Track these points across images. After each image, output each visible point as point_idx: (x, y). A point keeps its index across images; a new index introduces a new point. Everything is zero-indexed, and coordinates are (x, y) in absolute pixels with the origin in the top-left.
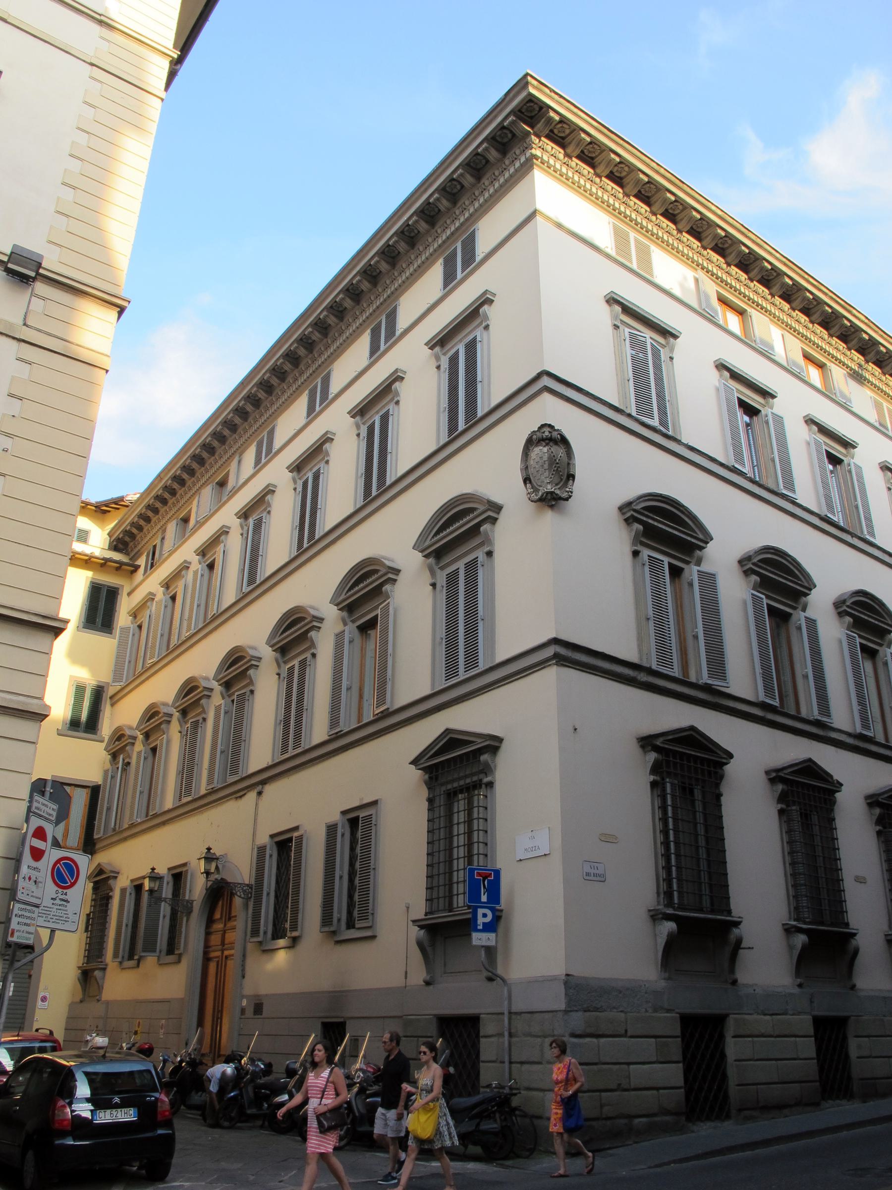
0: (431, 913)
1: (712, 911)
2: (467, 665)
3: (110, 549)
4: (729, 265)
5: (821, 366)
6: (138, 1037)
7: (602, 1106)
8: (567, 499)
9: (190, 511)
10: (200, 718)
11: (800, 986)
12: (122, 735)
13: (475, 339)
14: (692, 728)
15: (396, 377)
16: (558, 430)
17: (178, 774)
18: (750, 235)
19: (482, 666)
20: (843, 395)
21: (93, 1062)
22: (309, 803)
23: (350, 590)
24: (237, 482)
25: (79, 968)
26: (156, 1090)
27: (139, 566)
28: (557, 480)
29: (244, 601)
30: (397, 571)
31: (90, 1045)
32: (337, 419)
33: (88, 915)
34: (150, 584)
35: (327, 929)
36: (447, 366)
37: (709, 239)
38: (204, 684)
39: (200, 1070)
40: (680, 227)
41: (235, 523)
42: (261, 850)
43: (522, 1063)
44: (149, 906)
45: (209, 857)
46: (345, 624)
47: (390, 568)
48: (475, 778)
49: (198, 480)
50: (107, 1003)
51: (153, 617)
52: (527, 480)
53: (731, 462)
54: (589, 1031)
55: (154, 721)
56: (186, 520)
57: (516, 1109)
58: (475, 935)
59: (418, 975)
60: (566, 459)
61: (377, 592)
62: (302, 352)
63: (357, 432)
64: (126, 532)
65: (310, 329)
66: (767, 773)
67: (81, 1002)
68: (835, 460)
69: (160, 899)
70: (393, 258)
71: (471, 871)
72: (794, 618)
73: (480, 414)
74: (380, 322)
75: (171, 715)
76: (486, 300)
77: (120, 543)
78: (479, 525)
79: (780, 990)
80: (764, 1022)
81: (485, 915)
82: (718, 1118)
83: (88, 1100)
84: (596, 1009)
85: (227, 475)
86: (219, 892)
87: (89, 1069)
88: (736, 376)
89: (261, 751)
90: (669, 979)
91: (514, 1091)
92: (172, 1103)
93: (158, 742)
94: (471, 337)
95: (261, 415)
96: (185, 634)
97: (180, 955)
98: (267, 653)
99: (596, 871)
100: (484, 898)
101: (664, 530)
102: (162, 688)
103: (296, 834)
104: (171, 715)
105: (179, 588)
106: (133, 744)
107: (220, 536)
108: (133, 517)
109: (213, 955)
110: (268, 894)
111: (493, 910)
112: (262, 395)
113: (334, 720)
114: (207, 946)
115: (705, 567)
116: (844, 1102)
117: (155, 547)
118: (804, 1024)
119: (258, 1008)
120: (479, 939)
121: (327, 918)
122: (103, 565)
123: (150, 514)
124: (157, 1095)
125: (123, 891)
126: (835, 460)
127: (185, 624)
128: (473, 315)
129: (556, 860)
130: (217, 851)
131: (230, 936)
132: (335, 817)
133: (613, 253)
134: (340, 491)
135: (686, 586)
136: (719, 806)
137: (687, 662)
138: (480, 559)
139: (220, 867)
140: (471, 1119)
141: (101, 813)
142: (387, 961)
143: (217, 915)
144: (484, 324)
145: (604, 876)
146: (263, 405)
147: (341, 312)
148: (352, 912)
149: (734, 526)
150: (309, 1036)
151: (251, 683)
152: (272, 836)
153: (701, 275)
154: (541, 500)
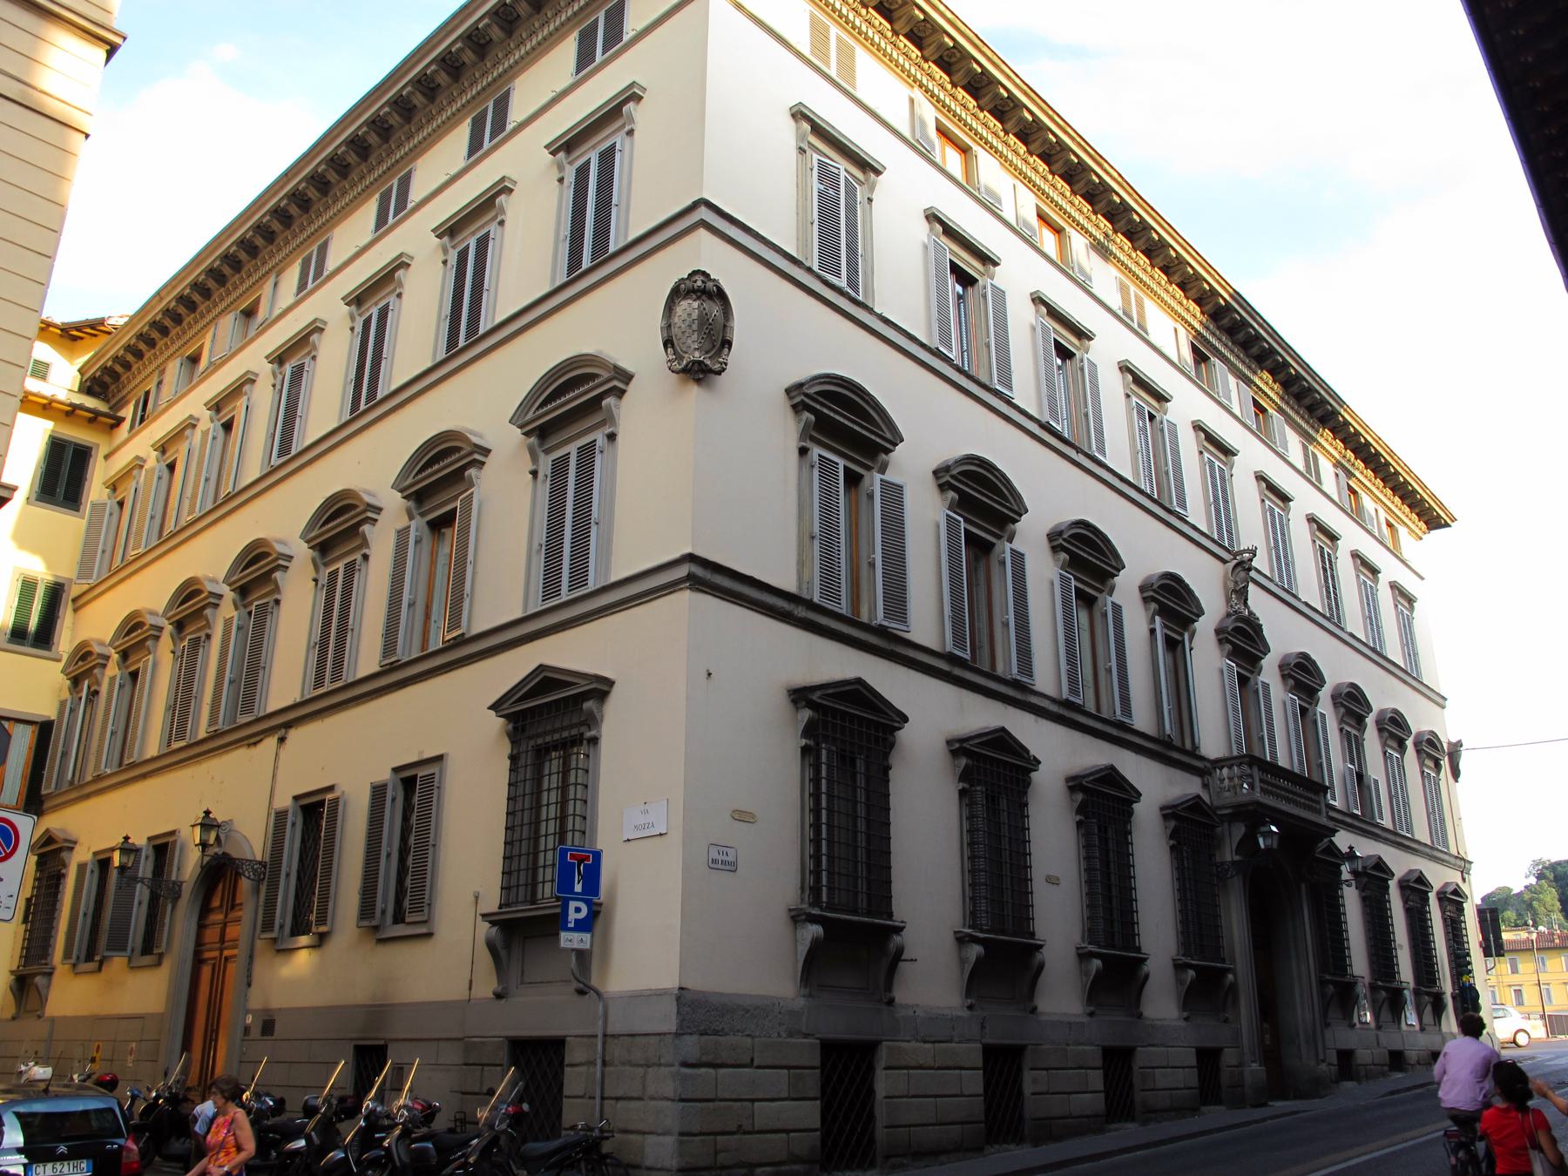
0: (507, 905)
1: (869, 913)
2: (572, 582)
3: (81, 390)
4: (954, 85)
5: (1058, 231)
6: (96, 1067)
7: (716, 1153)
8: (719, 373)
9: (202, 346)
10: (202, 634)
11: (970, 1007)
12: (90, 653)
13: (613, 147)
14: (859, 681)
15: (503, 188)
17: (167, 709)
18: (985, 49)
19: (592, 585)
20: (1082, 270)
21: (29, 1098)
22: (349, 756)
23: (420, 472)
24: (271, 312)
25: (12, 972)
26: (121, 1135)
27: (123, 419)
28: (707, 346)
29: (272, 478)
30: (486, 452)
31: (24, 1078)
32: (416, 237)
33: (28, 900)
34: (140, 445)
35: (366, 923)
36: (573, 180)
37: (1060, 164)
38: (210, 587)
39: (184, 1108)
40: (897, 27)
41: (265, 369)
42: (281, 816)
43: (618, 1099)
44: (119, 888)
45: (208, 823)
46: (411, 518)
47: (476, 446)
48: (574, 732)
49: (215, 305)
50: (53, 1020)
51: (141, 492)
52: (668, 343)
53: (934, 343)
54: (704, 1059)
55: (136, 636)
56: (194, 360)
57: (607, 1156)
58: (564, 935)
59: (487, 985)
60: (721, 319)
61: (457, 478)
62: (373, 139)
63: (531, 467)
64: (105, 370)
65: (387, 109)
66: (949, 742)
67: (14, 1018)
68: (1064, 353)
69: (135, 879)
70: (511, 22)
71: (563, 853)
72: (997, 549)
73: (612, 249)
74: (486, 110)
75: (161, 629)
76: (632, 95)
77: (92, 386)
78: (601, 397)
79: (947, 1012)
80: (922, 1052)
81: (578, 910)
82: (861, 1167)
83: (19, 1151)
84: (716, 1033)
85: (257, 301)
86: (220, 871)
87: (22, 1109)
88: (950, 232)
89: (286, 681)
90: (810, 996)
91: (605, 1135)
92: (143, 1153)
93: (141, 665)
94: (607, 144)
95: (311, 222)
96: (186, 518)
97: (161, 956)
98: (302, 552)
100: (578, 888)
101: (842, 423)
102: (151, 591)
103: (329, 796)
104: (161, 629)
105: (180, 453)
106: (104, 666)
107: (242, 385)
108: (117, 349)
109: (207, 955)
110: (288, 875)
111: (589, 903)
112: (313, 193)
113: (389, 646)
114: (199, 943)
115: (890, 476)
116: (1012, 1146)
117: (147, 394)
118: (972, 1053)
119: (268, 1027)
120: (570, 940)
121: (367, 908)
122: (71, 413)
123: (142, 346)
124: (121, 1141)
125: (82, 867)
126: (1064, 353)
127: (186, 503)
128: (613, 114)
129: (676, 836)
130: (219, 816)
131: (232, 931)
132: (385, 775)
133: (806, 51)
134: (415, 336)
135: (864, 499)
136: (886, 781)
137: (858, 596)
138: (599, 443)
139: (222, 837)
140: (547, 1169)
141: (53, 760)
142: (446, 964)
143: (216, 903)
144: (627, 128)
145: (734, 864)
146: (314, 208)
147: (433, 89)
148: (400, 903)
149: (934, 427)
150: (337, 1063)
151: (277, 589)
152: (296, 798)
153: (918, 94)
154: (685, 371)
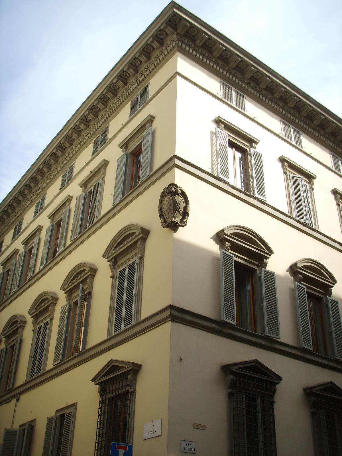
2: (127, 322)
14: (256, 361)
16: (179, 187)
48: (124, 390)
76: (151, 119)
99: (190, 447)
133: (222, 98)
